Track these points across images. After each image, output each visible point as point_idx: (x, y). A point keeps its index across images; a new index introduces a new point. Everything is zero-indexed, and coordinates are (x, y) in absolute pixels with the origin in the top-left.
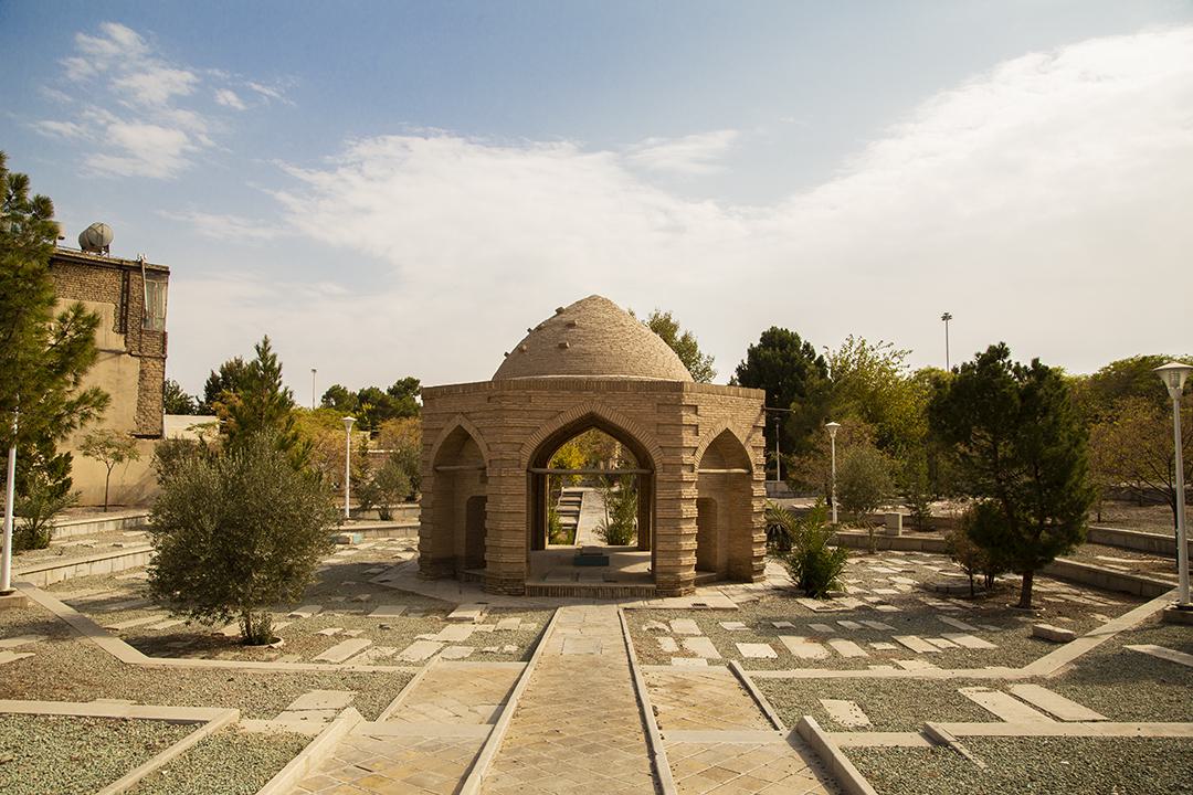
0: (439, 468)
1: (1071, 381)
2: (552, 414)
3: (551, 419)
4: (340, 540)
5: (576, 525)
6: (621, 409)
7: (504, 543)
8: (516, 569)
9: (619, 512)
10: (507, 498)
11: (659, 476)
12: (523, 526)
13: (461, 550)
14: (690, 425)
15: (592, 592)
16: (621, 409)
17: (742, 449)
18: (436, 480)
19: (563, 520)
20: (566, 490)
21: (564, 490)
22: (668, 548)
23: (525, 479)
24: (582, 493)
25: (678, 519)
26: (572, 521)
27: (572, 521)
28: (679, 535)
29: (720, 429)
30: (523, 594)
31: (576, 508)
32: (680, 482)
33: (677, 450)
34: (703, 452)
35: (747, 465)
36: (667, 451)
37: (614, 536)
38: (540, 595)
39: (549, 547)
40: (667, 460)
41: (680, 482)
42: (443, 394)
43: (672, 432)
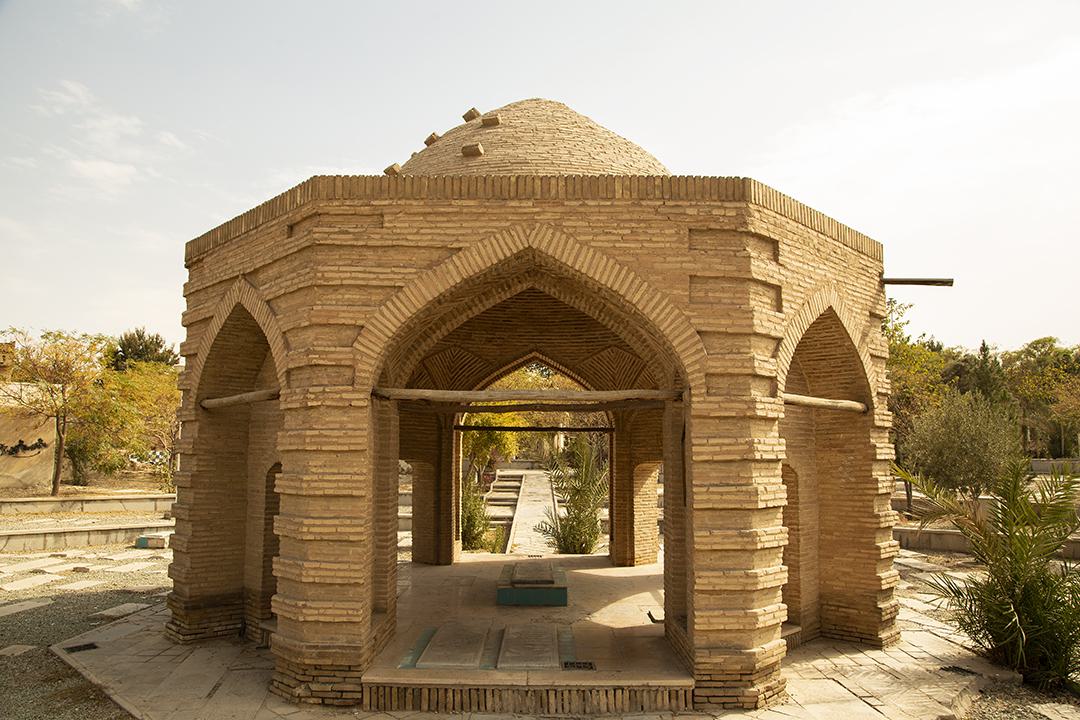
0: (207, 403)
1: (1009, 360)
2: (435, 255)
3: (429, 267)
4: (150, 543)
5: (511, 519)
6: (602, 242)
7: (311, 572)
8: (342, 641)
9: (577, 498)
10: (321, 460)
11: (699, 404)
12: (696, 470)
13: (399, 545)
14: (765, 284)
15: (530, 702)
16: (602, 242)
17: (854, 354)
18: (200, 430)
19: (493, 511)
20: (502, 473)
21: (499, 472)
22: (721, 583)
23: (367, 413)
24: (521, 477)
25: (747, 510)
26: (506, 512)
27: (506, 512)
28: (749, 550)
29: (820, 309)
30: (359, 703)
31: (513, 495)
32: (749, 418)
33: (738, 342)
34: (792, 350)
35: (862, 393)
36: (715, 342)
37: (570, 538)
38: (402, 707)
39: (461, 556)
40: (715, 366)
41: (749, 418)
42: (216, 244)
43: (726, 297)
